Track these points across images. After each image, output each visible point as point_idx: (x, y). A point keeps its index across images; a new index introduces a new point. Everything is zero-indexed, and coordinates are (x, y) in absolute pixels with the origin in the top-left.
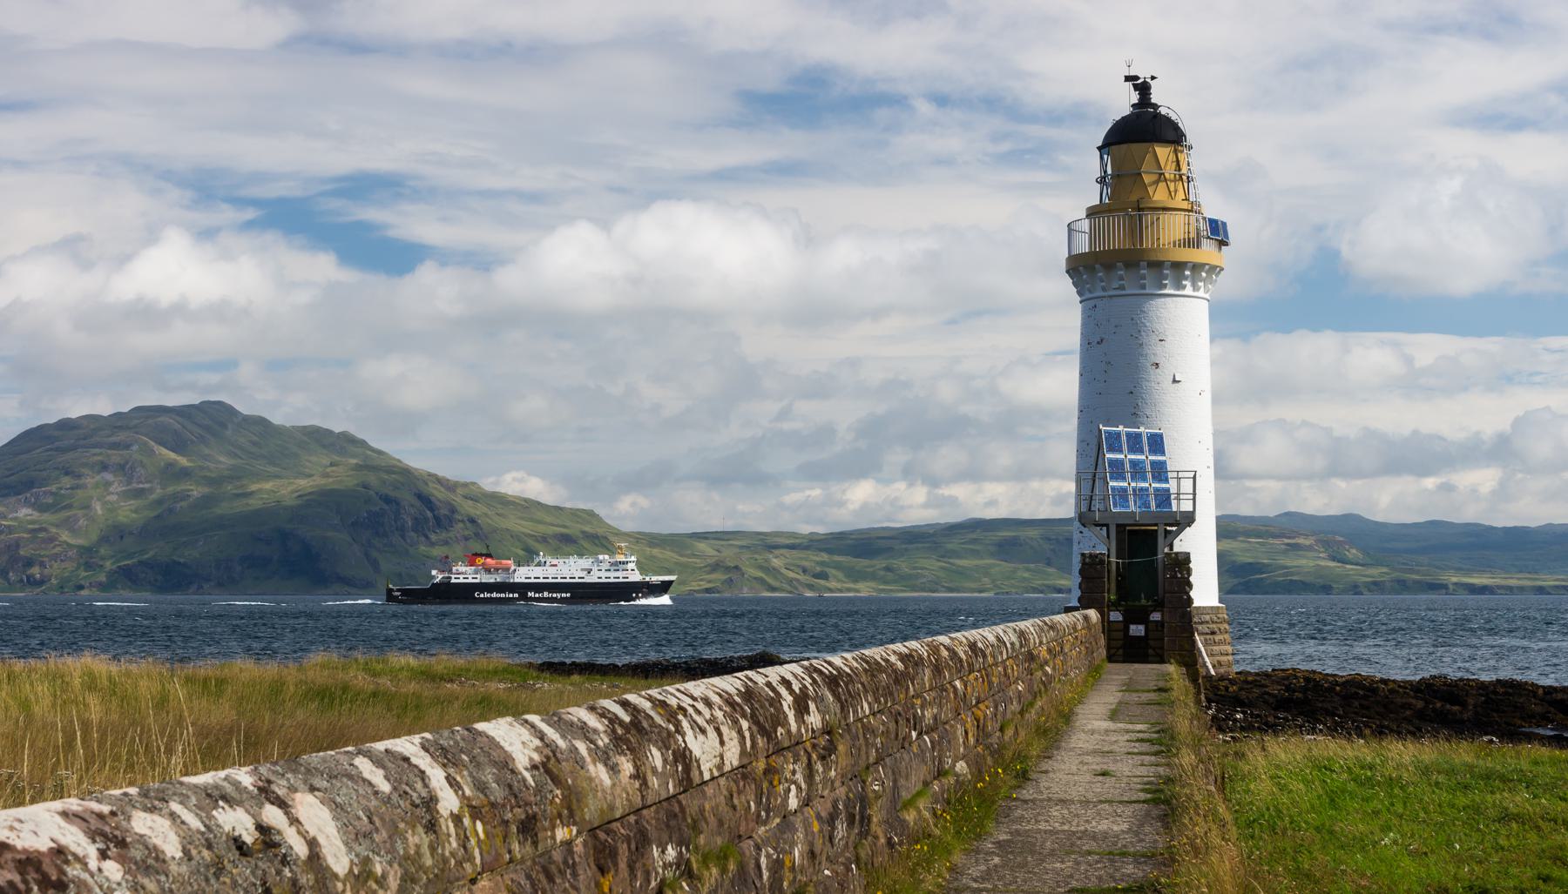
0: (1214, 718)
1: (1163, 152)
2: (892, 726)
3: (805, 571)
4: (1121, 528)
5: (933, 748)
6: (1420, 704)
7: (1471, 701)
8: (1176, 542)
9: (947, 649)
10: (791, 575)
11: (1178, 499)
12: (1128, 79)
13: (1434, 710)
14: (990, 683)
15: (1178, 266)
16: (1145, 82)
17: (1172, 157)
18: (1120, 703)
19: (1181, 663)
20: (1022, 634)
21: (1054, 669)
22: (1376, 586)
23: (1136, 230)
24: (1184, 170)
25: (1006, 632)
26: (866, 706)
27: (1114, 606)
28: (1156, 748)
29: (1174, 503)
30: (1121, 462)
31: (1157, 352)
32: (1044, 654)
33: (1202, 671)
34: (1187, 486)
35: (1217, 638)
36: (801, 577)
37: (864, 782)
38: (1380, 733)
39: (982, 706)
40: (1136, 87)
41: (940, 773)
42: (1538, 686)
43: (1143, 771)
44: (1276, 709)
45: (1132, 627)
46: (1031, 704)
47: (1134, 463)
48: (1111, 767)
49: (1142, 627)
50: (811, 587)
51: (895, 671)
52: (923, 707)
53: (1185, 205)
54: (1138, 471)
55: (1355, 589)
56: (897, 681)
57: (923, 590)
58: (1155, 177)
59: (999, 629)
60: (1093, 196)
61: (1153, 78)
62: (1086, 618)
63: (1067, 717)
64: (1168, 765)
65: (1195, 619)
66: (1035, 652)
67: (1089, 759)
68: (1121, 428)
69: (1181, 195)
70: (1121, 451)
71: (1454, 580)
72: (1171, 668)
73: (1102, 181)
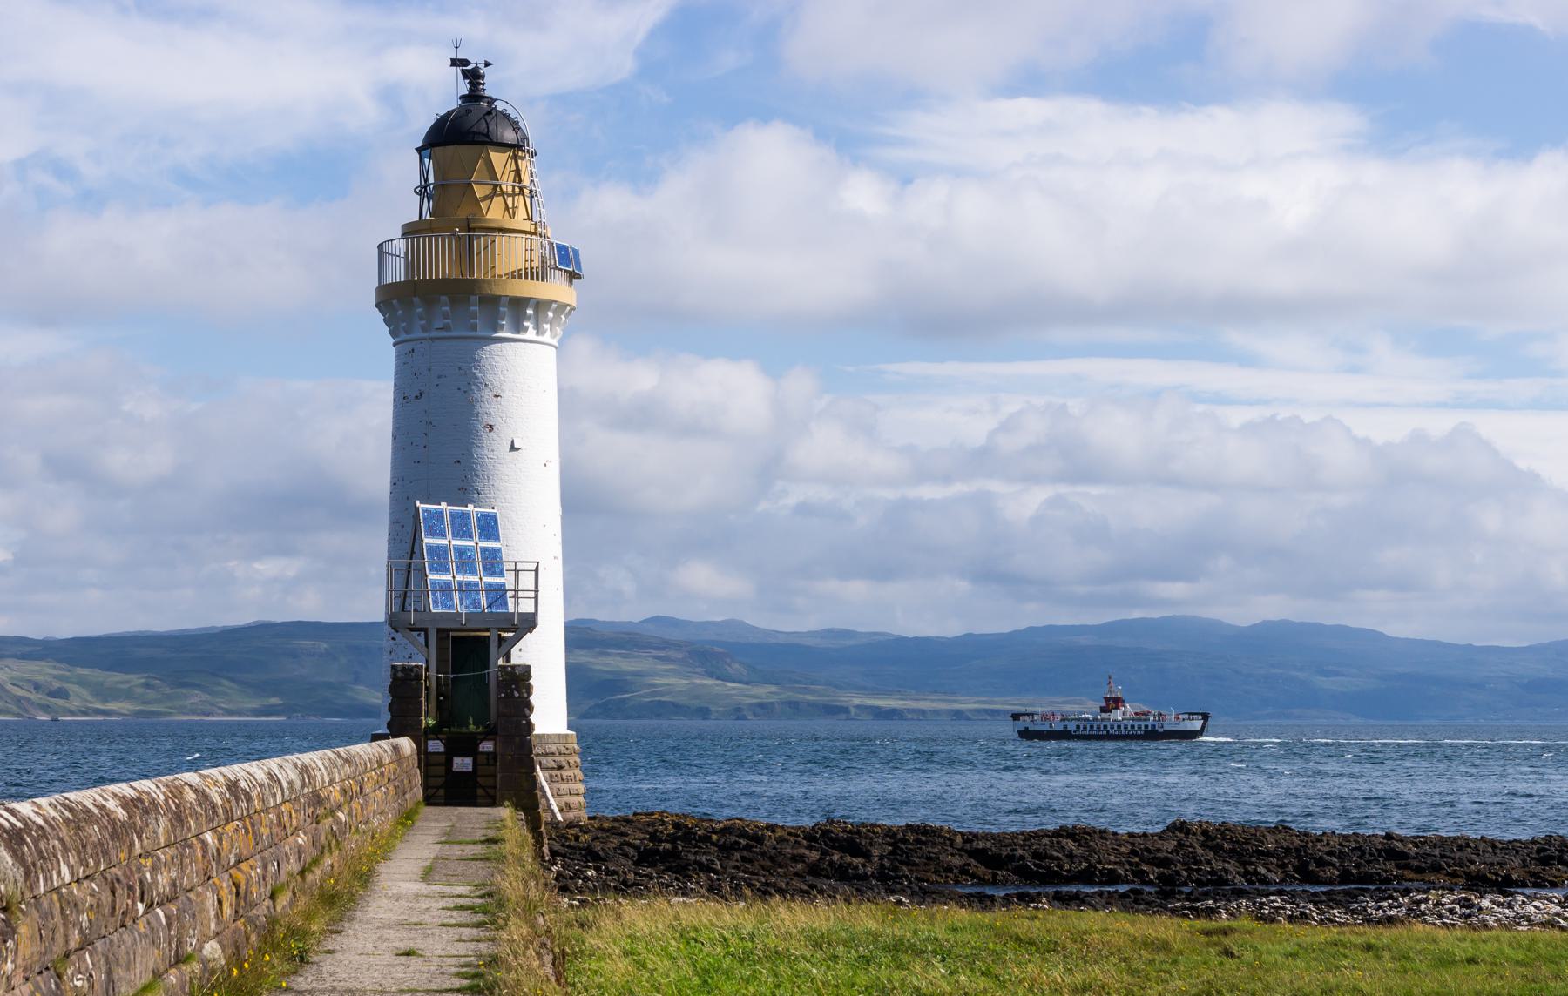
0: (559, 876)
1: (499, 159)
2: (106, 898)
3: (37, 687)
4: (443, 633)
5: (169, 925)
6: (814, 856)
7: (876, 852)
8: (514, 651)
9: (196, 791)
10: (20, 692)
11: (516, 597)
12: (454, 63)
13: (831, 863)
14: (257, 837)
15: (519, 304)
16: (476, 69)
17: (511, 165)
18: (436, 859)
19: (517, 806)
20: (304, 770)
21: (350, 814)
22: (764, 709)
23: (466, 254)
24: (526, 182)
25: (285, 767)
26: (65, 870)
27: (433, 732)
28: (480, 917)
29: (511, 602)
30: (444, 549)
31: (492, 410)
32: (336, 795)
33: (546, 817)
34: (527, 581)
35: (565, 773)
36: (33, 696)
37: (59, 976)
38: (764, 893)
39: (243, 866)
40: (465, 74)
41: (180, 960)
42: (955, 833)
43: (461, 949)
44: (637, 864)
45: (457, 761)
46: (316, 862)
47: (460, 551)
48: (418, 944)
49: (469, 761)
50: (45, 708)
51: (113, 822)
52: (154, 870)
53: (527, 226)
54: (465, 562)
55: (738, 712)
56: (115, 836)
57: (194, 713)
58: (488, 190)
59: (272, 764)
60: (410, 209)
61: (487, 64)
62: (396, 749)
63: (365, 878)
64: (493, 940)
65: (537, 750)
66: (323, 794)
67: (391, 933)
68: (443, 505)
69: (521, 213)
70: (443, 535)
71: (857, 701)
72: (505, 812)
73: (422, 190)
